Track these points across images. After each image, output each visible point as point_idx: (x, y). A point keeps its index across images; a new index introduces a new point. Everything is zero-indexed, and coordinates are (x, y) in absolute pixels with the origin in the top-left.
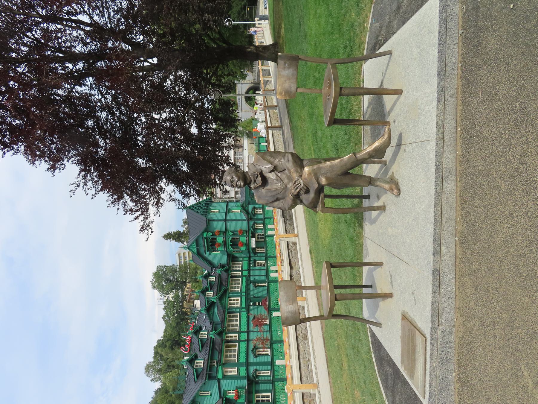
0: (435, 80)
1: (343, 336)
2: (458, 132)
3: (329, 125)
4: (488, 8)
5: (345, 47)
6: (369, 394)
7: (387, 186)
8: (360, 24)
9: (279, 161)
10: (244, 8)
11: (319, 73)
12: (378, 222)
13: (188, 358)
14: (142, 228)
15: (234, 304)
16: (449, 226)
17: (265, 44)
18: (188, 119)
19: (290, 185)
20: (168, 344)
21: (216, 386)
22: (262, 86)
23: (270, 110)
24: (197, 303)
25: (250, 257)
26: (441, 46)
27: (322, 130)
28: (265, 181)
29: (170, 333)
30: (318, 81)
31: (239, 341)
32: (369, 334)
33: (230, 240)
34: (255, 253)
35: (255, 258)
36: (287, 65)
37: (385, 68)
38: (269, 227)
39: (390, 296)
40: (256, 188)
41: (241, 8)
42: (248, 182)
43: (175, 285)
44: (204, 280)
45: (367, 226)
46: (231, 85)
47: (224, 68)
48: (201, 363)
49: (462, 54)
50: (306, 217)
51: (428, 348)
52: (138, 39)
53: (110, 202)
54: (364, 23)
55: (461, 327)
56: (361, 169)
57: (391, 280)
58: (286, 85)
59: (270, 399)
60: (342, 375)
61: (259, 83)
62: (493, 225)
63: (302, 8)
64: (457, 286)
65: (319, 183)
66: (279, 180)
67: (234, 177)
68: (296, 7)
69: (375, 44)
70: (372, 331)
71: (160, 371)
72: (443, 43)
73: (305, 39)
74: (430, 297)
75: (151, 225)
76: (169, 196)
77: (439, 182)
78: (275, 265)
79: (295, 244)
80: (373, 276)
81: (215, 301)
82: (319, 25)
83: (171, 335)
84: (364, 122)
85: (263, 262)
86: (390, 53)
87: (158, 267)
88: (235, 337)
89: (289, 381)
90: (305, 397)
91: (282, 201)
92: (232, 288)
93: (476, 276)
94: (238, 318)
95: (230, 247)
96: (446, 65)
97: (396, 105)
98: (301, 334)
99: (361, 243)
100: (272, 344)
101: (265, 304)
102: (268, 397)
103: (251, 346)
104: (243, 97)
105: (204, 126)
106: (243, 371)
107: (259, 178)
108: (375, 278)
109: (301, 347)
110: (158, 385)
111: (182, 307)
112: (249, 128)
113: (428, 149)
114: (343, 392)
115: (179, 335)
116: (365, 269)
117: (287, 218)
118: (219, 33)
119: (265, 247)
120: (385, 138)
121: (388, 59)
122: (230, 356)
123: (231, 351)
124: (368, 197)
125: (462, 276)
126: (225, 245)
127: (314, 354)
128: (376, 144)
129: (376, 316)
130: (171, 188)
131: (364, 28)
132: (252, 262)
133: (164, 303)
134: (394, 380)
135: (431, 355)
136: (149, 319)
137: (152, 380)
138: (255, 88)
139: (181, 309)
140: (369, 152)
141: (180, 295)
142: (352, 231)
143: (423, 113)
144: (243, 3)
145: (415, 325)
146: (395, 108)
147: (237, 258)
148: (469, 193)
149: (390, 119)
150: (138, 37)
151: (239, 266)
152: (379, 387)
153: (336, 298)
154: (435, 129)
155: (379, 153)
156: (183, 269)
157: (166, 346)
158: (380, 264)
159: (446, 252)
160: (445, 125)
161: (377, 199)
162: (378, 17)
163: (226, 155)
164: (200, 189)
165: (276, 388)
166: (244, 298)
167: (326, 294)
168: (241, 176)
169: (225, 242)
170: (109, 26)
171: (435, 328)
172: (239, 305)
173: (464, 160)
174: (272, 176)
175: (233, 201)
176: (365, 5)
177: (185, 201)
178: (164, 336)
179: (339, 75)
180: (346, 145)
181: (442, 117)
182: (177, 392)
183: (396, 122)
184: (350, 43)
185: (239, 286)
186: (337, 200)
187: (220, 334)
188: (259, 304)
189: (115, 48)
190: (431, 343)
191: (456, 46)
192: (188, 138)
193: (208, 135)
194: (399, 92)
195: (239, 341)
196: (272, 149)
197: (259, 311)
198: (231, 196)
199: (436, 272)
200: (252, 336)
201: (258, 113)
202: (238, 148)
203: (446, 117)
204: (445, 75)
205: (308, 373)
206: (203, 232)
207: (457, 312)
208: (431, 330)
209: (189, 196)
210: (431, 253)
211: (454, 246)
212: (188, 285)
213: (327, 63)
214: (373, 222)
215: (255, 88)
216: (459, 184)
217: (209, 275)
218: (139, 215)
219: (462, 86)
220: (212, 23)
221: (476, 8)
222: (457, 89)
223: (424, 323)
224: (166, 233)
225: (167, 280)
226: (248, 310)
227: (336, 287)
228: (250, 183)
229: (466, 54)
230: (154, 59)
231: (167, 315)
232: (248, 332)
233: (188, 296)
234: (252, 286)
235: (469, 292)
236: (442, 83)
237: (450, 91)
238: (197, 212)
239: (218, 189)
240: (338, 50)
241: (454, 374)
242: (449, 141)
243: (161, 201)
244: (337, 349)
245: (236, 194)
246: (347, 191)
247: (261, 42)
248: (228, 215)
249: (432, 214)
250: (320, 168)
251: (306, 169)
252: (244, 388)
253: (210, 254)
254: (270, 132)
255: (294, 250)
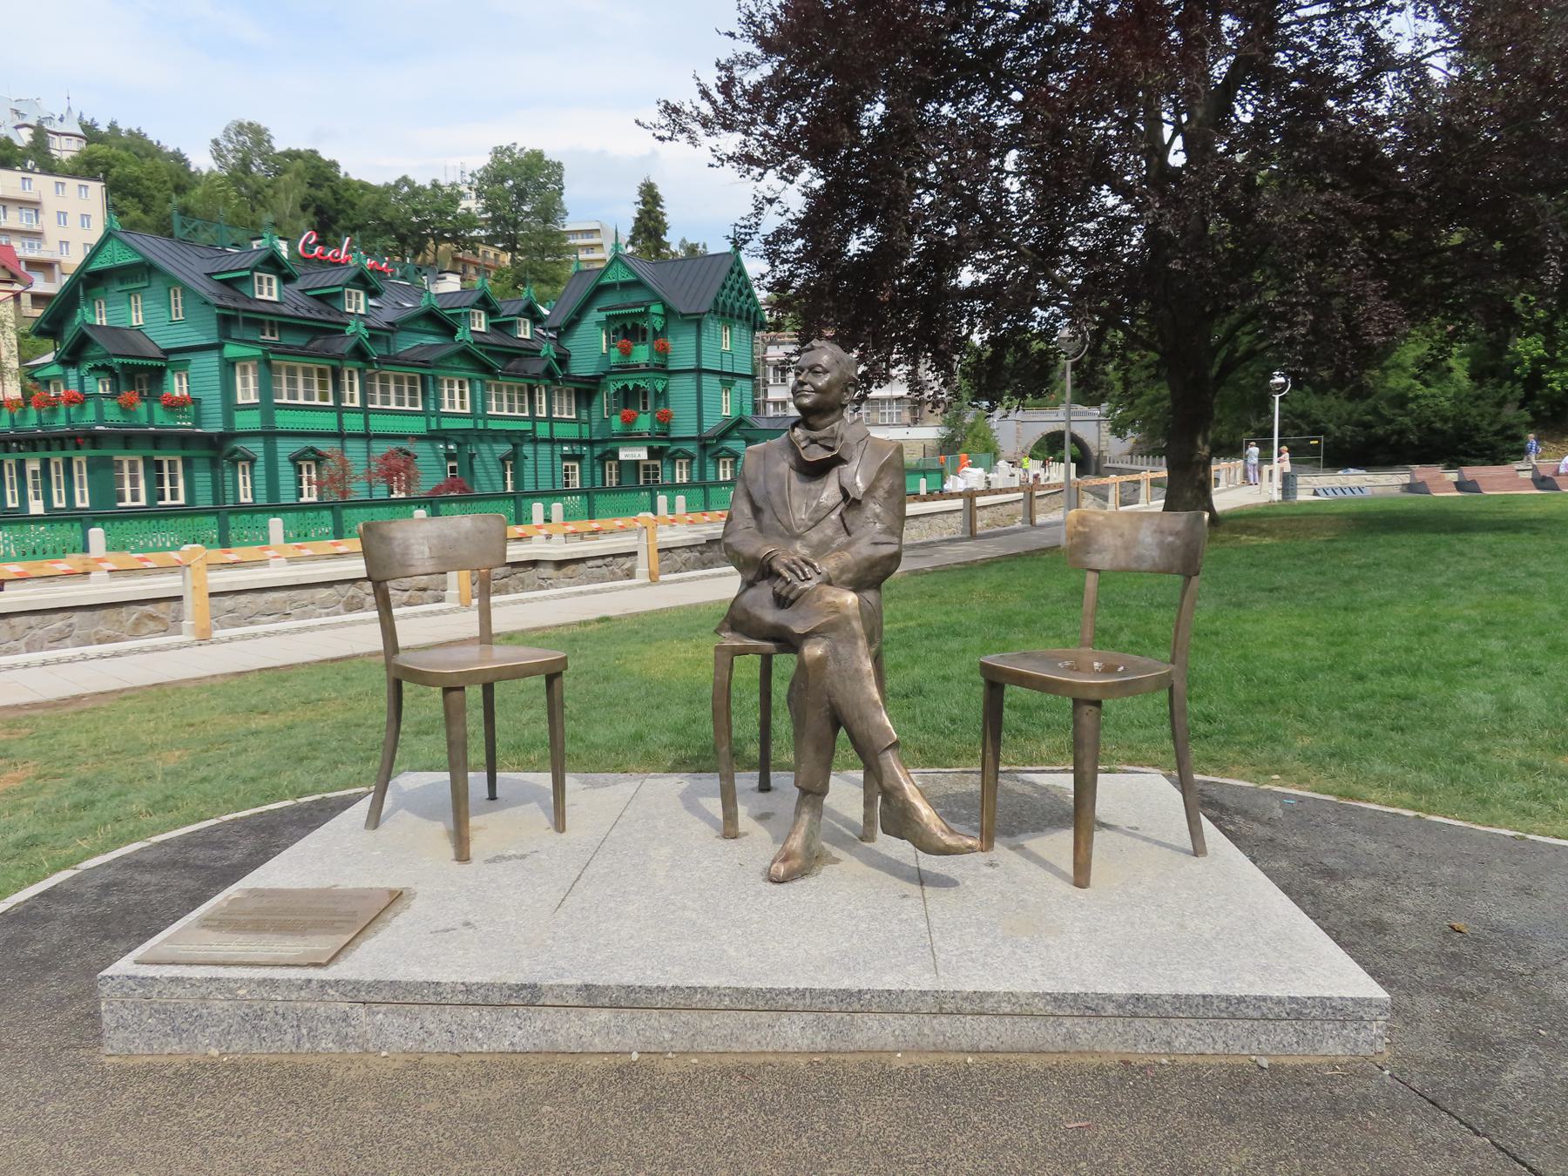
0: (1120, 988)
1: (348, 715)
2: (961, 1057)
3: (985, 669)
4: (1338, 1145)
5: (1209, 719)
6: (168, 793)
7: (796, 843)
8: (1279, 761)
9: (877, 516)
10: (1318, 431)
11: (1131, 643)
12: (687, 816)
13: (285, 255)
14: (676, 110)
15: (451, 394)
16: (672, 1032)
17: (1214, 490)
18: (1001, 257)
19: (801, 549)
20: (324, 194)
21: (203, 340)
22: (1093, 481)
23: (1021, 505)
24: (451, 284)
25: (591, 443)
26: (1224, 1005)
27: (964, 651)
28: (815, 471)
29: (361, 203)
30: (1107, 639)
31: (339, 410)
32: (352, 791)
33: (642, 384)
34: (603, 459)
35: (588, 457)
36: (1170, 539)
37: (1152, 835)
38: (680, 500)
39: (462, 855)
40: (793, 446)
41: (1316, 422)
42: (811, 420)
43: (503, 218)
44: (522, 305)
45: (675, 784)
46: (1096, 389)
47: (1147, 367)
48: (270, 294)
49: (1196, 1067)
50: (708, 605)
51: (293, 974)
52: (1243, 107)
53: (754, 10)
54: (1281, 773)
55: (363, 1070)
56: (849, 766)
57: (510, 858)
58: (1107, 539)
59: (168, 501)
60: (233, 711)
61: (1098, 473)
62: (675, 1168)
63: (1317, 595)
64: (488, 1059)
65: (806, 636)
66: (816, 517)
67: (827, 378)
68: (1321, 579)
69: (1222, 808)
70: (360, 797)
71: (245, 165)
72: (1232, 1008)
73: (1230, 603)
74: (454, 978)
75: (683, 137)
76: (769, 195)
77: (808, 1001)
78: (568, 516)
79: (630, 574)
80: (529, 801)
81: (458, 337)
82: (1272, 644)
83: (353, 206)
84: (990, 772)
85: (576, 482)
86: (1198, 849)
87: (559, 165)
88: (352, 396)
89: (217, 555)
90: (174, 604)
91: (753, 524)
92: (499, 389)
93: (519, 1118)
94: (407, 407)
95: (620, 385)
96: (1165, 1018)
97: (1041, 870)
98: (362, 594)
99: (625, 767)
100: (331, 507)
101: (452, 488)
102: (174, 496)
103: (323, 446)
104: (1061, 427)
105: (978, 306)
106: (247, 421)
107: (824, 455)
108: (519, 810)
109: (323, 593)
110: (202, 161)
111: (439, 239)
112: (969, 441)
113: (911, 968)
114: (183, 716)
115: (353, 230)
116: (545, 779)
117: (706, 553)
118: (1251, 354)
119: (620, 489)
120: (944, 837)
121: (1180, 845)
122: (292, 383)
123: (308, 384)
124: (765, 787)
125: (519, 1074)
126: (626, 369)
127: (299, 630)
128: (925, 811)
129: (401, 811)
130: (794, 201)
131: (1267, 773)
132: (577, 449)
133: (453, 185)
134: (205, 868)
135: (273, 984)
136: (405, 137)
137: (216, 142)
138: (1085, 462)
139: (432, 235)
140: (903, 789)
141: (474, 234)
142: (665, 739)
143: (1019, 951)
144: (1331, 426)
145: (368, 932)
146: (1032, 866)
147: (589, 405)
148: (776, 1093)
149: (1000, 850)
150: (1249, 108)
151: (565, 409)
152: (187, 824)
153: (452, 689)
154: (970, 988)
155: (900, 821)
156: (554, 244)
157: (319, 187)
158: (559, 824)
159: (593, 1024)
160: (984, 1018)
161: (758, 812)
162: (1302, 814)
163: (894, 372)
164: (791, 292)
165: (198, 520)
166: (468, 424)
167: (473, 660)
168: (830, 398)
169: (634, 369)
170: (1285, 19)
171: (357, 992)
172: (446, 409)
173: (877, 1076)
174: (829, 492)
175: (756, 395)
176: (1333, 777)
177: (756, 243)
178: (348, 184)
179: (1128, 700)
180: (920, 722)
181: (1008, 1010)
182: (177, 220)
183: (990, 870)
184: (1222, 732)
185: (504, 409)
186: (757, 698)
187: (359, 353)
188: (453, 469)
189: (1218, 38)
190: (310, 981)
191: (1220, 1047)
192: (945, 258)
193: (952, 318)
194: (1081, 876)
195: (339, 410)
196: (912, 508)
197: (430, 469)
198: (770, 390)
199: (529, 996)
200: (355, 449)
201: (1013, 470)
202: (913, 410)
203: (1007, 1020)
204: (1135, 1015)
205: (247, 612)
206: (664, 304)
207: (408, 1057)
208: (349, 982)
209: (773, 256)
210: (589, 980)
211: (611, 1048)
212: (506, 258)
213: (1173, 662)
214: (690, 802)
215: (1085, 462)
216: (802, 1062)
217: (537, 319)
218: (713, 103)
219: (1100, 1068)
220: (1287, 333)
221: (1335, 1108)
222: (1093, 1052)
223: (369, 961)
224: (660, 191)
225: (522, 196)
226: (433, 436)
227: (488, 689)
228: (810, 427)
229: (1198, 1078)
230: (1182, 155)
231: (416, 192)
232: (367, 436)
233: (473, 258)
234: (504, 448)
235: (468, 1096)
236: (1110, 1009)
237: (1085, 1032)
238: (724, 287)
239: (791, 349)
240: (1199, 697)
241: (214, 1052)
242: (934, 1029)
243: (757, 171)
244: (313, 697)
245: (776, 403)
246: (782, 724)
247: (1217, 480)
248: (715, 380)
249: (711, 983)
250: (853, 638)
251: (850, 598)
252: (198, 423)
253: (599, 323)
254: (958, 503)
255: (613, 573)
